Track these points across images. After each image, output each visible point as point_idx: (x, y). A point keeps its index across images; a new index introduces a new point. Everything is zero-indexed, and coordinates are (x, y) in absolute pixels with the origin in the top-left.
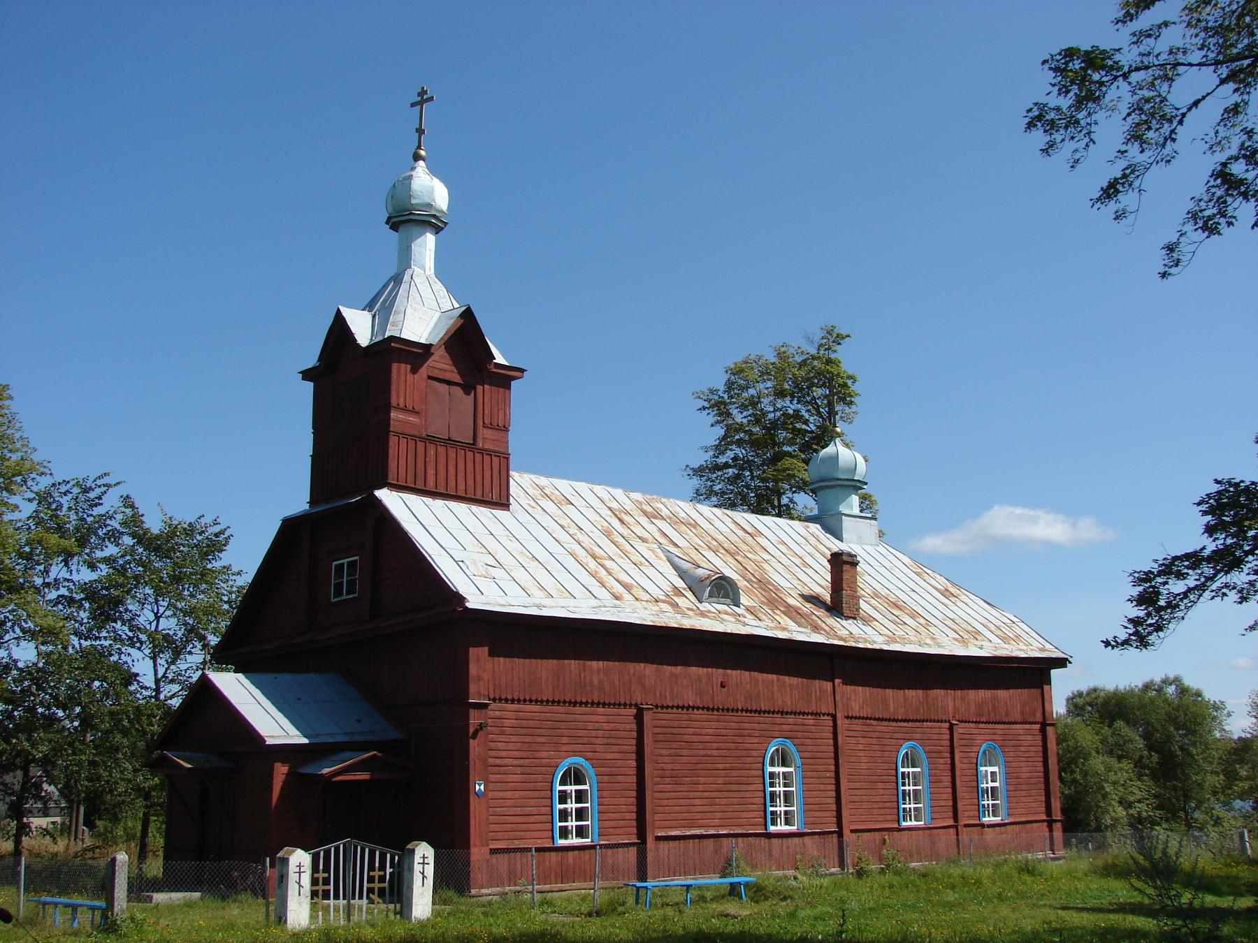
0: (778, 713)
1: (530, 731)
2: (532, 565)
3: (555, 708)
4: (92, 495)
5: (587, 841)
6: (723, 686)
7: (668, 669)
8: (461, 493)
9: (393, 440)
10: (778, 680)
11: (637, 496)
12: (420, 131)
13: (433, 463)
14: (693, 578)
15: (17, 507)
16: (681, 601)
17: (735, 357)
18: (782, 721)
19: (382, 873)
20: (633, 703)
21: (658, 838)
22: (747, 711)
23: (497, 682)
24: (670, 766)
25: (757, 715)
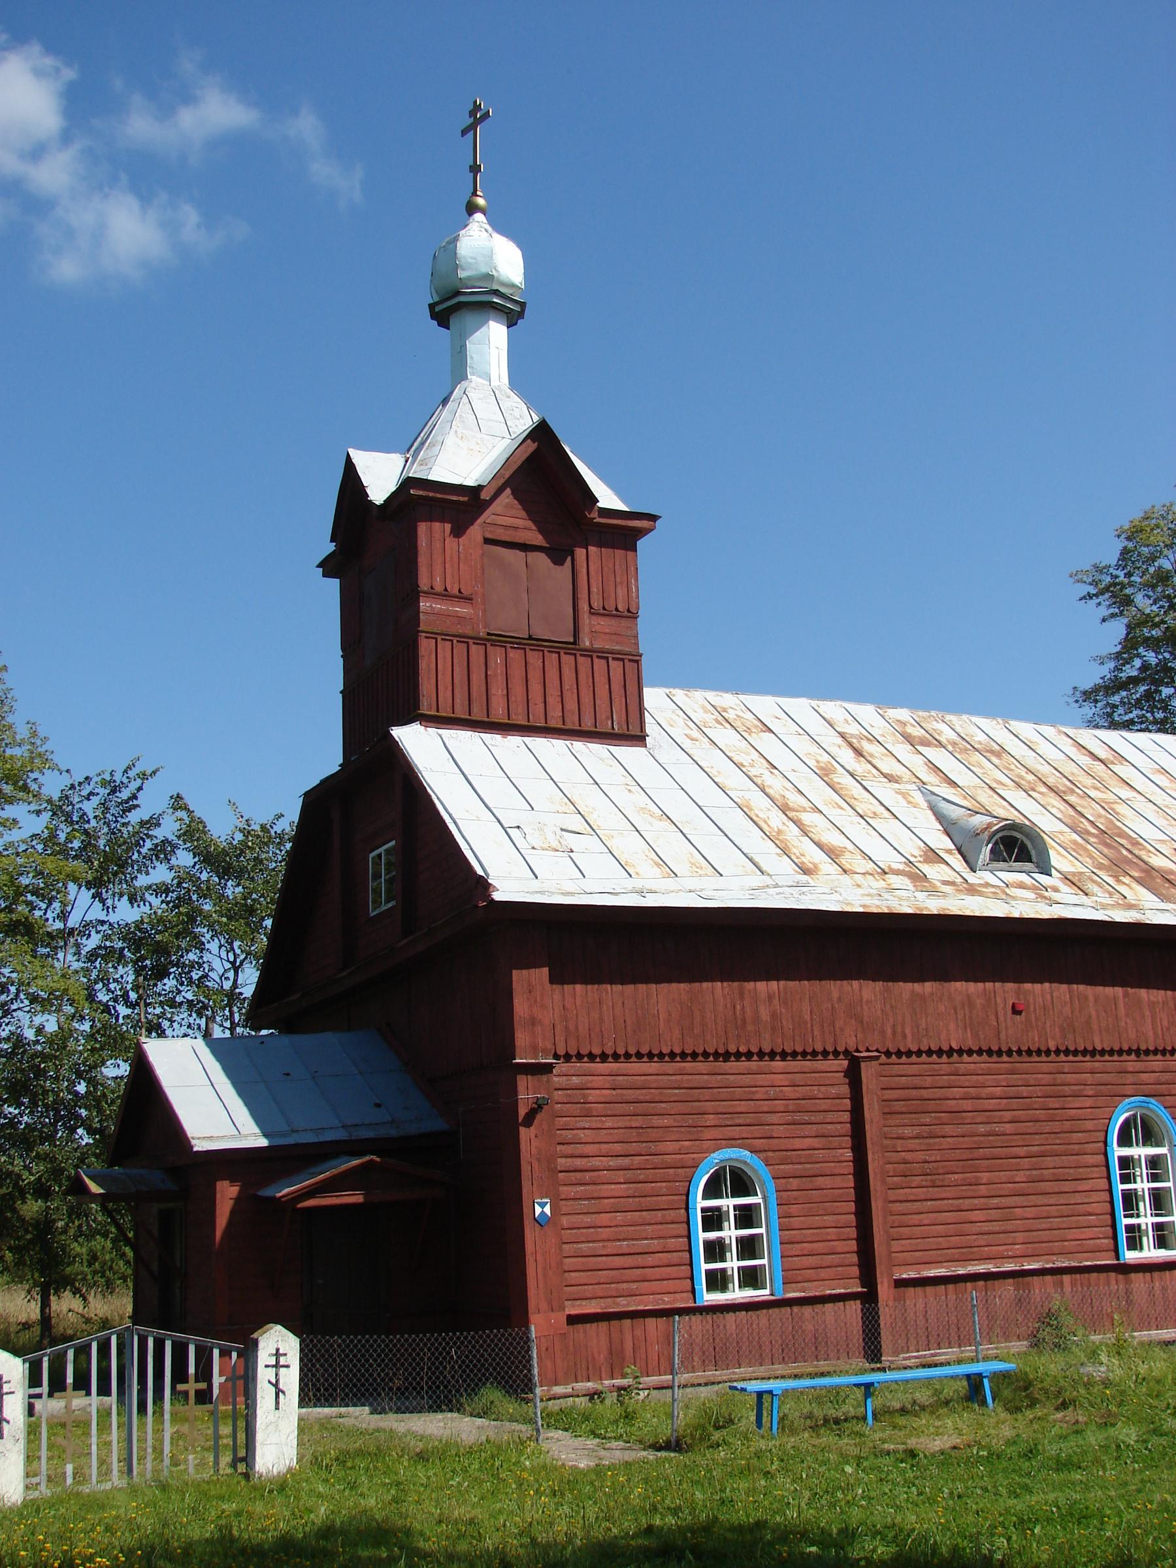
0: (1129, 1052)
1: (640, 1108)
2: (656, 830)
3: (689, 1066)
4: (125, 794)
5: (763, 1294)
6: (1016, 1011)
7: (905, 989)
8: (554, 723)
9: (425, 646)
10: (1126, 995)
11: (903, 714)
12: (475, 169)
13: (501, 679)
14: (964, 831)
15: (15, 821)
16: (934, 872)
17: (1130, 515)
18: (1139, 1066)
19: (203, 1386)
20: (841, 1049)
21: (901, 1283)
22: (1067, 1052)
23: (572, 1027)
24: (920, 1156)
25: (1088, 1058)
